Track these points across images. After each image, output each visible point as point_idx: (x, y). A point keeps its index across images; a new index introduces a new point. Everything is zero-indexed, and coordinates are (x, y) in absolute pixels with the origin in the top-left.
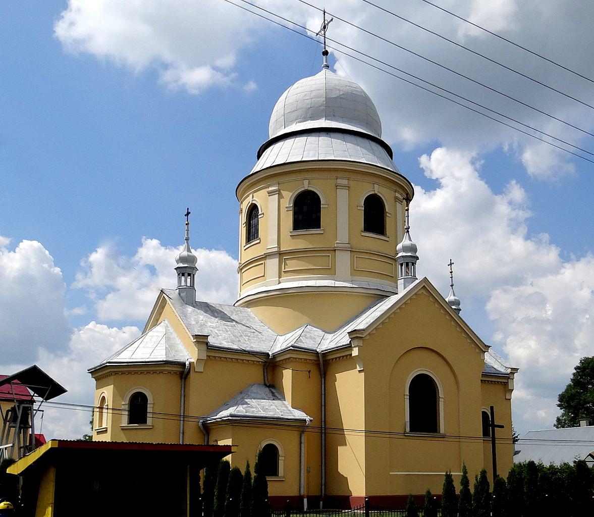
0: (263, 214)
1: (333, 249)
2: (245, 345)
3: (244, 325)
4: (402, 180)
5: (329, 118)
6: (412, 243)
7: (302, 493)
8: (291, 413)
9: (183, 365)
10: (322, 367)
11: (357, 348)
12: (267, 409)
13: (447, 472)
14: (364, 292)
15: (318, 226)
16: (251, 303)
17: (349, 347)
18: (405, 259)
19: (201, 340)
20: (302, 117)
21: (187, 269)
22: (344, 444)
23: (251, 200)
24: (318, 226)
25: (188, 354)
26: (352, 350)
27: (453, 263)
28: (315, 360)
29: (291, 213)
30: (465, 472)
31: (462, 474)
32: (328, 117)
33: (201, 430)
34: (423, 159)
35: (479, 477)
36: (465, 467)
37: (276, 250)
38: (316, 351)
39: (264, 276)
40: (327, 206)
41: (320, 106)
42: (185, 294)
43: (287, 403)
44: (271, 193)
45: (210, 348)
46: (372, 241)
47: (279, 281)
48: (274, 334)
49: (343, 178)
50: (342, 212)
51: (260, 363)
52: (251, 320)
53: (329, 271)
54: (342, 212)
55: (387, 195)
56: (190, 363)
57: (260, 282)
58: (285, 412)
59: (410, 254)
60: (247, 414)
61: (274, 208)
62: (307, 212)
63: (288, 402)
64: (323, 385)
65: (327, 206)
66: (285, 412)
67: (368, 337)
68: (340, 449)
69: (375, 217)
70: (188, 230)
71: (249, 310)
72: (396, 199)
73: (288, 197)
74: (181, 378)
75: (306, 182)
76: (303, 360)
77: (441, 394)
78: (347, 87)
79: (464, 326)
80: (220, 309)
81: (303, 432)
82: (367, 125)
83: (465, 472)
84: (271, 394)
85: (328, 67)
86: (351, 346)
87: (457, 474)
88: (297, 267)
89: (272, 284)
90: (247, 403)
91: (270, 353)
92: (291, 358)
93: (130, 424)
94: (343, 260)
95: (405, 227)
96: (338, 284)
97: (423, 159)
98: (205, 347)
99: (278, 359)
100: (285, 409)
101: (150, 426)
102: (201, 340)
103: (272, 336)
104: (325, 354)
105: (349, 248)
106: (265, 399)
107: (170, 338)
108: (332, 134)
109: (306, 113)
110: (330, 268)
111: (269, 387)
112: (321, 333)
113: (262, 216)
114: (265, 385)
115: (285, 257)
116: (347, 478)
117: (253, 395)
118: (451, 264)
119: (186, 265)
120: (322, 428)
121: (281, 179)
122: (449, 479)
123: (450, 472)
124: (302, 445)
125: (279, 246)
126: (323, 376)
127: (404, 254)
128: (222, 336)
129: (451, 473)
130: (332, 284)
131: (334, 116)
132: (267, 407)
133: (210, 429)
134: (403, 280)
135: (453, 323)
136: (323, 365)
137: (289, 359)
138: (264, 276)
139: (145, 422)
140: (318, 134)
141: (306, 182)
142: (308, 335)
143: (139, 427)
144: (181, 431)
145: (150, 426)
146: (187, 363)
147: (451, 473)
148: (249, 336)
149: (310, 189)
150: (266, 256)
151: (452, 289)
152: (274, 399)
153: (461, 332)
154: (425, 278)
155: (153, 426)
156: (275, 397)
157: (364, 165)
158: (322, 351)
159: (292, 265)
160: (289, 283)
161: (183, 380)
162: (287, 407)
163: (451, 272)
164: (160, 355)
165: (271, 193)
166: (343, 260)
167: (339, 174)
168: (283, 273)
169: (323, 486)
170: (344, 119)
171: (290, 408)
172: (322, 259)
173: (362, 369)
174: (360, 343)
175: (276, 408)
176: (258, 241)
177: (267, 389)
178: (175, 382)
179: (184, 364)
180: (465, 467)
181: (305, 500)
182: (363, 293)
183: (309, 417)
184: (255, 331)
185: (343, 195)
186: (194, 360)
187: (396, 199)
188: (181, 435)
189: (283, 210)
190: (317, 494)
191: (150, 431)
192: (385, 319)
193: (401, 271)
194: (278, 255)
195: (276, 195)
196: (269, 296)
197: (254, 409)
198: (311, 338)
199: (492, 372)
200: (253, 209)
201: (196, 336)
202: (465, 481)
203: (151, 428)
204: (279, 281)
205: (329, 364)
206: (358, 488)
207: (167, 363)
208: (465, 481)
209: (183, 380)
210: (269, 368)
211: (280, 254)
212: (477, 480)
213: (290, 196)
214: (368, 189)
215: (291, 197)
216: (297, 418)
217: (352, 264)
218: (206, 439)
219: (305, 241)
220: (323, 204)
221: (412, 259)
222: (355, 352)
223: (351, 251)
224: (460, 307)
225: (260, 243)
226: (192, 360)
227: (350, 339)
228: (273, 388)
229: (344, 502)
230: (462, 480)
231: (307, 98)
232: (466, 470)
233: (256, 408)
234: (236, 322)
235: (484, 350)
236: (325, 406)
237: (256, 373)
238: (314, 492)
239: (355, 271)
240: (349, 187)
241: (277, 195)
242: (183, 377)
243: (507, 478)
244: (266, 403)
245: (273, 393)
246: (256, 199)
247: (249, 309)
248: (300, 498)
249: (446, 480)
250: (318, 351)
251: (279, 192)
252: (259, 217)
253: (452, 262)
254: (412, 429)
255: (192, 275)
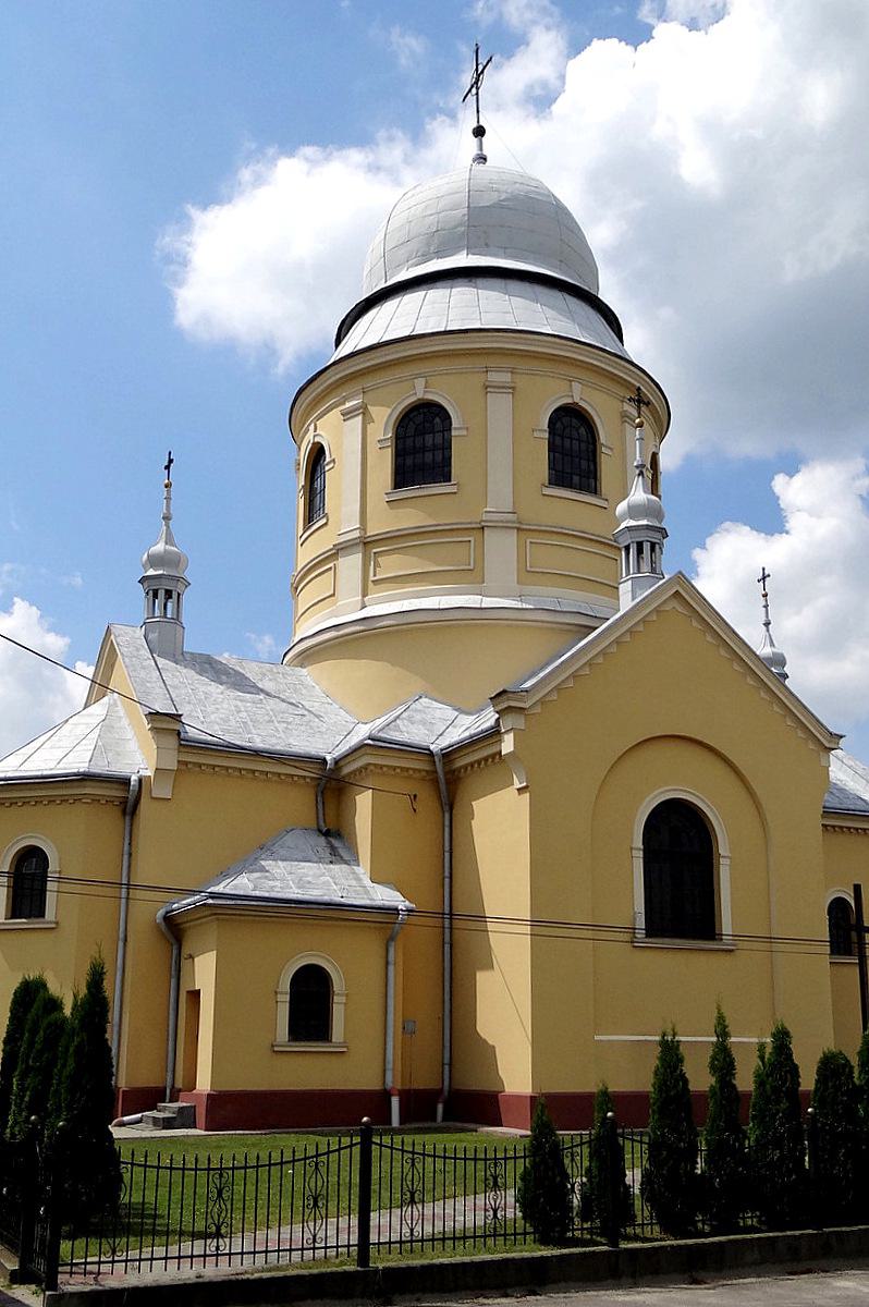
0: (334, 460)
1: (479, 526)
2: (274, 741)
3: (283, 701)
4: (641, 377)
5: (476, 250)
6: (775, 650)
7: (389, 1084)
8: (367, 892)
9: (124, 782)
10: (443, 787)
11: (512, 735)
12: (309, 882)
13: (664, 1035)
14: (548, 619)
15: (447, 478)
16: (308, 657)
17: (494, 734)
18: (634, 534)
19: (165, 724)
20: (419, 254)
21: (164, 581)
22: (488, 965)
23: (313, 434)
24: (447, 478)
25: (137, 758)
26: (500, 741)
27: (769, 576)
28: (427, 771)
29: (388, 454)
30: (723, 1033)
31: (714, 1039)
32: (471, 250)
33: (163, 934)
34: (779, 482)
35: (769, 1050)
36: (721, 1019)
37: (356, 534)
38: (429, 750)
39: (333, 595)
40: (465, 433)
41: (456, 227)
42: (156, 634)
43: (363, 871)
44: (348, 415)
45: (186, 745)
46: (568, 507)
47: (363, 602)
48: (349, 718)
49: (499, 370)
50: (499, 446)
51: (308, 780)
52: (304, 691)
53: (471, 576)
54: (499, 446)
55: (604, 409)
56: (140, 780)
57: (325, 609)
58: (351, 889)
59: (645, 522)
60: (257, 893)
61: (356, 443)
62: (422, 448)
63: (363, 870)
64: (447, 830)
65: (465, 433)
66: (351, 889)
67: (538, 710)
68: (481, 977)
69: (573, 453)
70: (168, 499)
71: (304, 671)
72: (624, 416)
73: (383, 419)
74: (124, 813)
75: (420, 383)
76: (398, 770)
77: (723, 847)
78: (517, 185)
79: (743, 652)
80: (238, 668)
81: (392, 938)
82: (562, 263)
83: (723, 1033)
84: (328, 851)
85: (485, 159)
86: (498, 733)
87: (697, 1040)
88: (401, 569)
89: (347, 609)
90: (263, 869)
91: (328, 758)
92: (370, 764)
93: (11, 918)
94: (501, 549)
95: (635, 464)
96: (488, 602)
97: (779, 482)
98: (172, 742)
99: (346, 771)
100: (354, 883)
101: (51, 922)
102: (165, 724)
103: (326, 717)
104: (449, 755)
105: (514, 522)
106: (309, 861)
107: (113, 727)
108: (480, 282)
109: (428, 245)
110: (471, 567)
111: (327, 834)
112: (450, 713)
113: (332, 465)
114: (320, 831)
115: (375, 550)
116: (494, 1047)
117: (283, 852)
118: (764, 578)
119: (161, 572)
120: (444, 928)
121: (369, 382)
122: (671, 1055)
123: (674, 1036)
124: (391, 968)
125: (363, 527)
126: (446, 808)
127: (633, 523)
128: (214, 714)
129: (677, 1038)
130: (476, 603)
131: (487, 245)
132: (309, 879)
133: (184, 930)
134: (630, 582)
135: (723, 652)
136: (447, 779)
137: (366, 767)
138: (333, 595)
139: (42, 914)
140: (450, 282)
141: (420, 383)
142: (418, 717)
143: (26, 926)
144: (121, 936)
145: (51, 922)
146: (134, 778)
147: (677, 1038)
148: (288, 723)
149: (582, 404)
150: (339, 550)
151: (768, 631)
152: (331, 862)
153: (785, 716)
154: (680, 572)
155: (57, 923)
156: (335, 856)
157: (550, 339)
158: (442, 750)
159: (391, 565)
160: (384, 605)
161: (128, 818)
162: (358, 879)
163: (765, 596)
164: (78, 763)
165: (348, 413)
166: (501, 549)
167: (492, 362)
168: (371, 585)
169: (447, 1067)
170: (508, 251)
171: (367, 882)
172: (455, 548)
173: (525, 784)
174: (518, 721)
175: (331, 880)
176: (324, 521)
177: (322, 840)
178: (110, 820)
179: (125, 782)
180: (721, 1019)
181: (395, 1101)
182: (548, 622)
183: (407, 903)
184: (306, 713)
185: (500, 405)
186: (150, 773)
187: (624, 416)
188: (121, 944)
189: (373, 447)
190: (437, 1087)
191: (51, 935)
192: (580, 668)
193: (626, 563)
194: (361, 547)
195: (356, 419)
196: (342, 636)
197: (278, 883)
198: (423, 722)
199: (858, 808)
200: (318, 453)
201: (154, 716)
202: (723, 1062)
203: (53, 928)
204: (363, 602)
205: (459, 779)
206: (516, 1075)
207: (85, 778)
208: (723, 1062)
209: (128, 818)
210: (325, 792)
211: (365, 543)
212: (762, 1058)
213: (387, 415)
214: (554, 393)
215: (390, 415)
216: (379, 903)
217: (522, 557)
218: (175, 952)
219: (420, 509)
220: (455, 429)
221: (651, 533)
222: (507, 745)
223: (518, 529)
224: (787, 669)
225: (326, 524)
226: (143, 773)
227: (497, 716)
228: (333, 836)
229: (482, 1106)
230: (714, 1058)
231: (429, 212)
232: (726, 1027)
233: (282, 880)
234: (268, 694)
235: (827, 745)
236: (451, 878)
237: (299, 803)
238: (424, 1080)
239: (529, 574)
240: (513, 388)
241: (360, 417)
242: (128, 810)
243: (859, 1053)
244: (309, 870)
245: (333, 848)
246: (321, 433)
247: (305, 670)
248: (385, 1095)
249: (662, 1059)
250: (432, 747)
251: (363, 410)
252: (327, 468)
253: (766, 573)
254: (653, 930)
255: (175, 595)
